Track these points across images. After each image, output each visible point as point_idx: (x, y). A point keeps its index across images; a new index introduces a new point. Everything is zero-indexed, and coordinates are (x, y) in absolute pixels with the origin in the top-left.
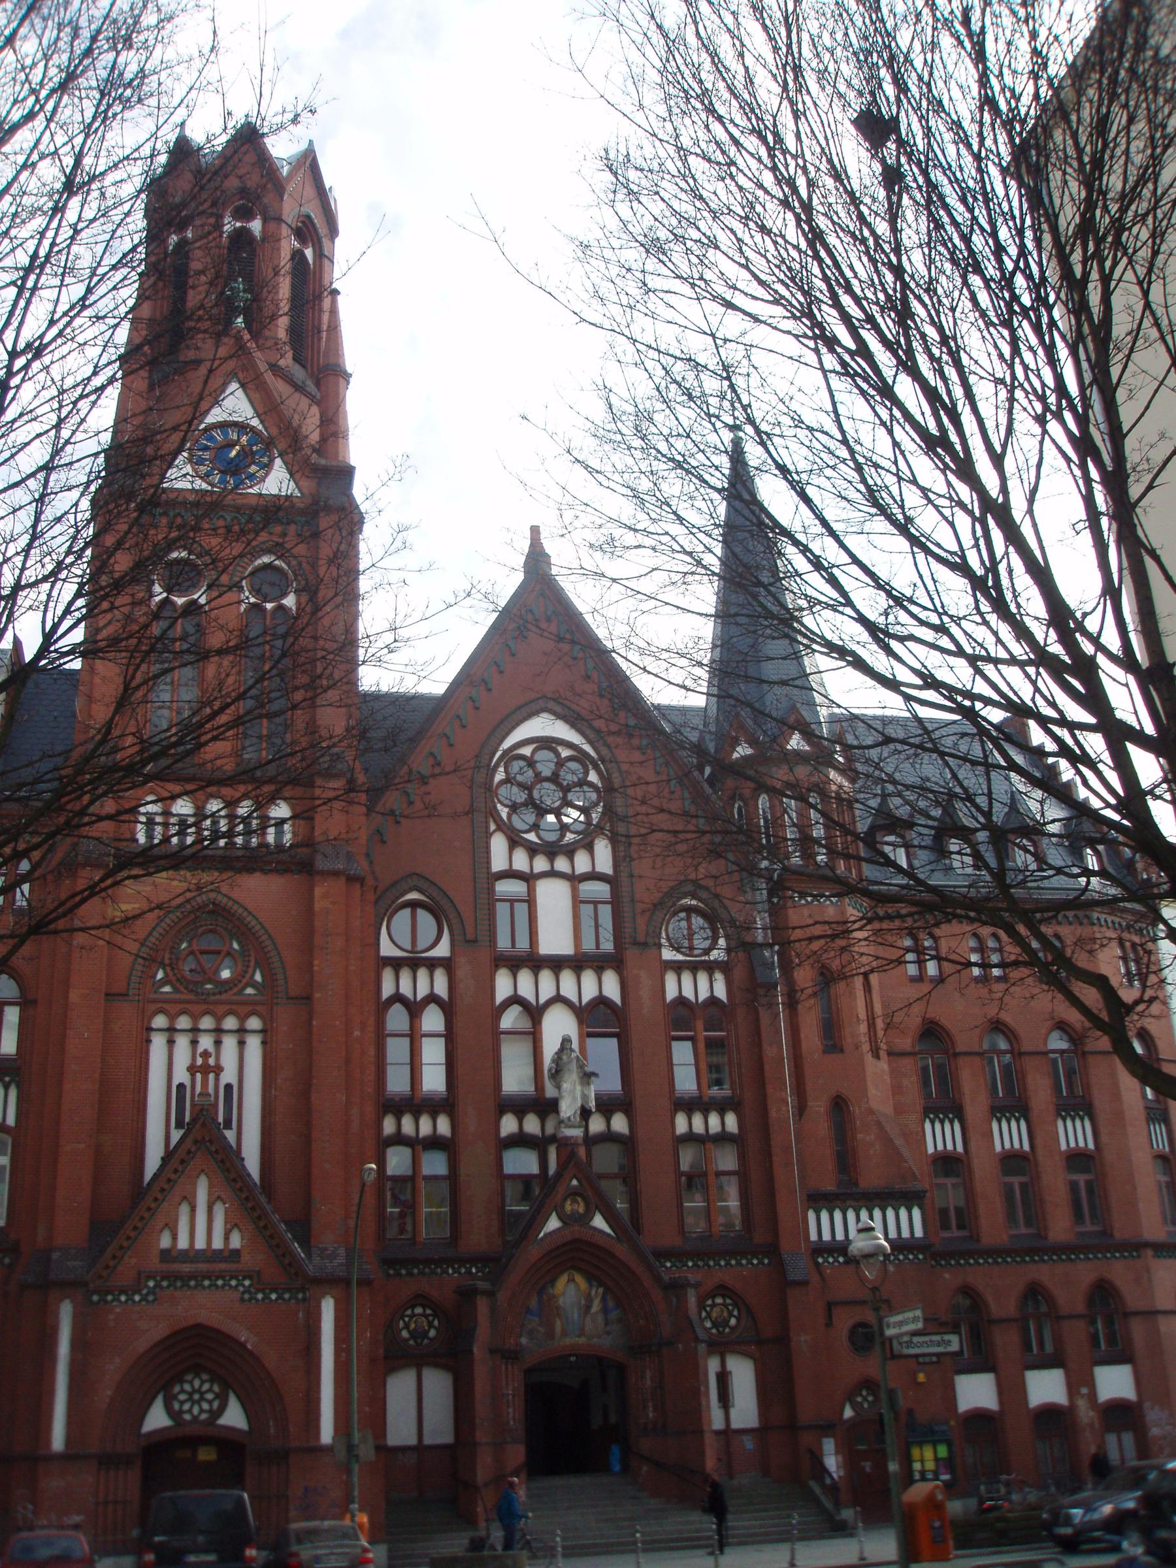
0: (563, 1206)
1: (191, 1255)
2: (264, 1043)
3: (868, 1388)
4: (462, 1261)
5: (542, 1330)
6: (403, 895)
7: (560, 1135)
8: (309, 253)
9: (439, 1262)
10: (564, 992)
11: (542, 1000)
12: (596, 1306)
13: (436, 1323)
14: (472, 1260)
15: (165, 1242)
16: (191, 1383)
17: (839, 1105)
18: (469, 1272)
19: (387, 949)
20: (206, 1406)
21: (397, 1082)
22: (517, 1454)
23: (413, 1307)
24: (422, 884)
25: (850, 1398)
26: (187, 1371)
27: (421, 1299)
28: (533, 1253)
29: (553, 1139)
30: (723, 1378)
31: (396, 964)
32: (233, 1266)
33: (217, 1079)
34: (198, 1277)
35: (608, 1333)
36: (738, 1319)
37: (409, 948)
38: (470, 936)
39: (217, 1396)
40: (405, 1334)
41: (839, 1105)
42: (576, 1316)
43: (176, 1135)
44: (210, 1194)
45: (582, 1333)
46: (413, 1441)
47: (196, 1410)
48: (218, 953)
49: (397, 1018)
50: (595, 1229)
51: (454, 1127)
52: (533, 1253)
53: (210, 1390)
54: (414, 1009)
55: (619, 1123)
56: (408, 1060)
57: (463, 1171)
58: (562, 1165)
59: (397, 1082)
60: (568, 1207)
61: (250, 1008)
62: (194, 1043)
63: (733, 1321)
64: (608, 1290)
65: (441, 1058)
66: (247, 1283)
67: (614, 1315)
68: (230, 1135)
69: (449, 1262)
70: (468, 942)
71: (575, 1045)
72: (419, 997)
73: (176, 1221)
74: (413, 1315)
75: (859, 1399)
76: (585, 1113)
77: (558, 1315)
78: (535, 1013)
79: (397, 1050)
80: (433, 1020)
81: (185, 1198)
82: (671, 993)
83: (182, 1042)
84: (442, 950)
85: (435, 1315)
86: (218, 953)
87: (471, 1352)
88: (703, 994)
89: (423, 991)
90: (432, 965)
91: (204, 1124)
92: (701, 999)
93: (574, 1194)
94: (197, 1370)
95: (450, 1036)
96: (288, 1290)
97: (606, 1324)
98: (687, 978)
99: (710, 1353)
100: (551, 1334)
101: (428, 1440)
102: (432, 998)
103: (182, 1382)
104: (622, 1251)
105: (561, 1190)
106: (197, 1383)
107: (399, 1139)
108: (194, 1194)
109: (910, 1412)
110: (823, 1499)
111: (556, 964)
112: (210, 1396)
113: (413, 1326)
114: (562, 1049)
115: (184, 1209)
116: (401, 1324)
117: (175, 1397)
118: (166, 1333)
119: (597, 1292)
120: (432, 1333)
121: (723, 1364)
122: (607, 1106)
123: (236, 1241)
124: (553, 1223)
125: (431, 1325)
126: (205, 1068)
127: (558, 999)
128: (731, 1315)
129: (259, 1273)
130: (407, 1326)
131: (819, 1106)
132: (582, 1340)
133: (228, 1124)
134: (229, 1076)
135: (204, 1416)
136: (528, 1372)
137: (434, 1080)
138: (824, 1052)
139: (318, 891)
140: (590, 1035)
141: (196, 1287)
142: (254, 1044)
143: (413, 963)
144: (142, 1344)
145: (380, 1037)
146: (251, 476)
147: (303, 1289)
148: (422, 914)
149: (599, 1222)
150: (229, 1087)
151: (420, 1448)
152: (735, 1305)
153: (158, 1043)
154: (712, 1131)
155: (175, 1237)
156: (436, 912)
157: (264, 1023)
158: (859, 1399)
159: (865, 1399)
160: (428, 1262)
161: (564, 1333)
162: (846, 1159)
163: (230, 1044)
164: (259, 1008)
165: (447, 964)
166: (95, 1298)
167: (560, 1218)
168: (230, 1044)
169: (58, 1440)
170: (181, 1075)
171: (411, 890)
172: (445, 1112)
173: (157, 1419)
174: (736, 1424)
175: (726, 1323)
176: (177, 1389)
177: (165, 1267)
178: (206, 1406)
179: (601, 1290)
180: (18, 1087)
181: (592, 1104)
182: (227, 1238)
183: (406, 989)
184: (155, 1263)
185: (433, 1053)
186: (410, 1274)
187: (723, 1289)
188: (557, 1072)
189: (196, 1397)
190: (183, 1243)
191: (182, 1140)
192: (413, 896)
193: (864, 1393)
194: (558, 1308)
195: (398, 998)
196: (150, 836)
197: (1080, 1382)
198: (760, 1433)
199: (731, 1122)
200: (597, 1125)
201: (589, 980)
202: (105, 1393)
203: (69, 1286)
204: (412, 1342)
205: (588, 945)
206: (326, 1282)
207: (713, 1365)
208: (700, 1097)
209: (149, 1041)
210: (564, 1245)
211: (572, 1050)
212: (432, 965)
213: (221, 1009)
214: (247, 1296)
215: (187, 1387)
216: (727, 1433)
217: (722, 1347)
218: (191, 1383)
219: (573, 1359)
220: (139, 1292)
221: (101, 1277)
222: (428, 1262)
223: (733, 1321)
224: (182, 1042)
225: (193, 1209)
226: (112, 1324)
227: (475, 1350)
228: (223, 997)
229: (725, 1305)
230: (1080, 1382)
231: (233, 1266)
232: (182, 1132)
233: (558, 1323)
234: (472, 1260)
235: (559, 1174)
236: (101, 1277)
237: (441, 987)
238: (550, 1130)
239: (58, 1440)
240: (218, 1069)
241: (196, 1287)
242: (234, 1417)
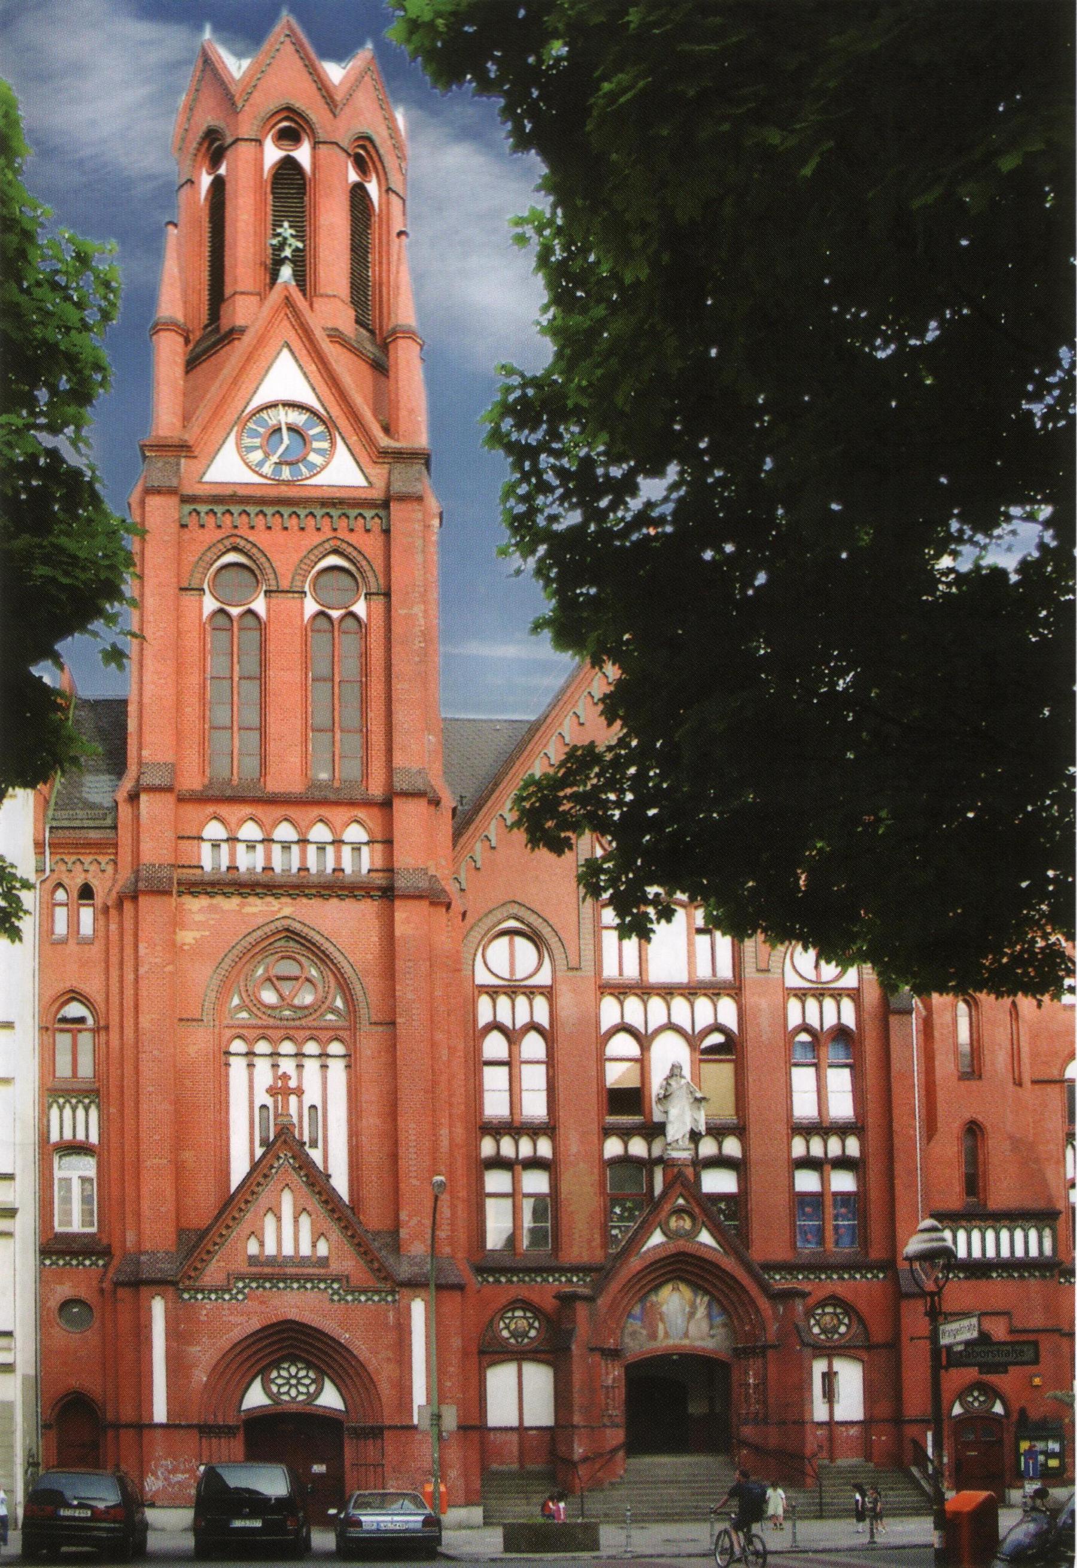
0: (667, 1223)
1: (272, 1261)
2: (348, 1067)
3: (979, 1390)
4: (563, 1270)
5: (644, 1332)
6: (500, 923)
7: (666, 1157)
8: (373, 188)
9: (539, 1270)
10: (676, 1019)
11: (651, 1028)
12: (701, 1312)
13: (536, 1324)
14: (575, 1270)
15: (253, 1248)
16: (288, 1370)
17: (974, 1130)
18: (570, 1281)
19: (482, 977)
20: (303, 1389)
21: (496, 1106)
22: (616, 1436)
23: (513, 1310)
24: (515, 909)
25: (961, 1396)
26: (283, 1359)
27: (526, 1305)
28: (635, 1264)
29: (660, 1160)
30: (829, 1377)
31: (493, 992)
32: (322, 1271)
33: (300, 1103)
34: (296, 1278)
35: (713, 1336)
36: (848, 1326)
37: (507, 976)
38: (573, 963)
39: (313, 1381)
40: (505, 1334)
41: (974, 1130)
42: (679, 1321)
43: (259, 1152)
44: (295, 1206)
45: (686, 1335)
46: (515, 1423)
47: (293, 1392)
48: (296, 979)
49: (495, 1046)
50: (701, 1244)
51: (555, 1149)
52: (635, 1264)
53: (307, 1376)
54: (512, 1036)
55: (732, 1147)
56: (506, 1086)
57: (564, 1188)
58: (668, 1186)
59: (496, 1106)
60: (673, 1223)
61: (332, 1033)
62: (275, 1066)
63: (843, 1329)
64: (714, 1299)
65: (542, 1083)
66: (336, 1286)
67: (719, 1320)
68: (316, 1155)
69: (551, 1270)
70: (572, 969)
71: (686, 1071)
72: (518, 1026)
73: (262, 1228)
74: (513, 1317)
75: (970, 1399)
76: (695, 1137)
77: (662, 1320)
78: (644, 1040)
79: (495, 1079)
80: (533, 1046)
81: (270, 1209)
82: (794, 1019)
83: (263, 1066)
84: (544, 978)
85: (536, 1318)
86: (296, 979)
87: (569, 1349)
88: (830, 1021)
89: (522, 1019)
90: (530, 992)
91: (285, 1142)
92: (826, 1027)
93: (679, 1211)
94: (293, 1360)
95: (551, 1062)
96: (377, 1292)
97: (711, 1327)
98: (812, 1004)
99: (816, 1357)
100: (653, 1336)
101: (527, 1423)
102: (533, 1026)
103: (279, 1368)
104: (729, 1263)
105: (667, 1207)
106: (293, 1370)
107: (498, 1163)
108: (279, 1204)
109: (1023, 1412)
110: (923, 1483)
111: (667, 992)
112: (307, 1381)
113: (513, 1326)
114: (672, 1075)
115: (270, 1222)
116: (502, 1325)
117: (273, 1381)
118: (258, 1326)
119: (702, 1303)
120: (533, 1333)
121: (830, 1366)
122: (718, 1132)
123: (323, 1249)
124: (657, 1238)
125: (531, 1326)
126: (281, 1090)
127: (671, 1027)
128: (841, 1323)
129: (347, 1277)
130: (507, 1327)
131: (950, 1126)
132: (686, 1342)
133: (314, 1144)
134: (312, 1096)
135: (301, 1398)
136: (629, 1369)
137: (535, 1107)
138: (960, 1079)
139: (399, 916)
140: (701, 1061)
141: (285, 1288)
142: (337, 1071)
143: (512, 989)
144: (236, 1334)
145: (477, 1063)
146: (311, 466)
147: (392, 1292)
148: (521, 942)
149: (705, 1237)
150: (313, 1107)
151: (521, 1429)
152: (846, 1313)
153: (237, 1067)
154: (830, 1155)
155: (262, 1244)
156: (534, 937)
157: (347, 1048)
158: (970, 1399)
159: (976, 1399)
160: (528, 1270)
161: (667, 1335)
162: (973, 1183)
163: (312, 1066)
164: (341, 1033)
165: (548, 992)
166: (186, 1296)
167: (665, 1233)
168: (312, 1066)
169: (160, 1413)
170: (262, 1098)
171: (509, 918)
172: (545, 1134)
173: (256, 1397)
174: (839, 1416)
175: (835, 1330)
176: (274, 1374)
177: (254, 1270)
178: (293, 1392)
179: (706, 1299)
180: (98, 1107)
181: (702, 1128)
182: (314, 1245)
183: (505, 1018)
184: (244, 1268)
185: (534, 1078)
186: (510, 1281)
187: (834, 1300)
188: (666, 1097)
189: (293, 1381)
190: (270, 1249)
191: (264, 1155)
192: (512, 924)
193: (976, 1394)
194: (660, 1314)
195: (496, 1026)
196: (216, 859)
197: (719, 550)
198: (867, 1424)
199: (853, 1147)
200: (708, 1148)
201: (703, 1004)
202: (200, 1376)
203: (161, 1284)
204: (512, 1341)
205: (703, 972)
206: (415, 1285)
207: (819, 1367)
208: (821, 1122)
209: (228, 1065)
210: (667, 1257)
211: (682, 1077)
212: (530, 992)
213: (301, 1035)
214: (336, 1297)
215: (284, 1373)
216: (831, 1424)
217: (830, 1351)
218: (288, 1370)
219: (675, 1357)
220: (229, 1291)
221: (190, 1277)
222: (528, 1270)
223: (843, 1329)
224: (263, 1066)
225: (279, 1219)
226: (203, 1318)
227: (573, 1347)
228: (303, 1022)
229: (835, 1314)
230: (719, 550)
231: (322, 1271)
232: (263, 1149)
233: (661, 1326)
234: (575, 1270)
235: (664, 1193)
236: (190, 1277)
237: (542, 1017)
238: (656, 1152)
239: (160, 1413)
240: (299, 1092)
241: (285, 1288)
242: (330, 1398)
